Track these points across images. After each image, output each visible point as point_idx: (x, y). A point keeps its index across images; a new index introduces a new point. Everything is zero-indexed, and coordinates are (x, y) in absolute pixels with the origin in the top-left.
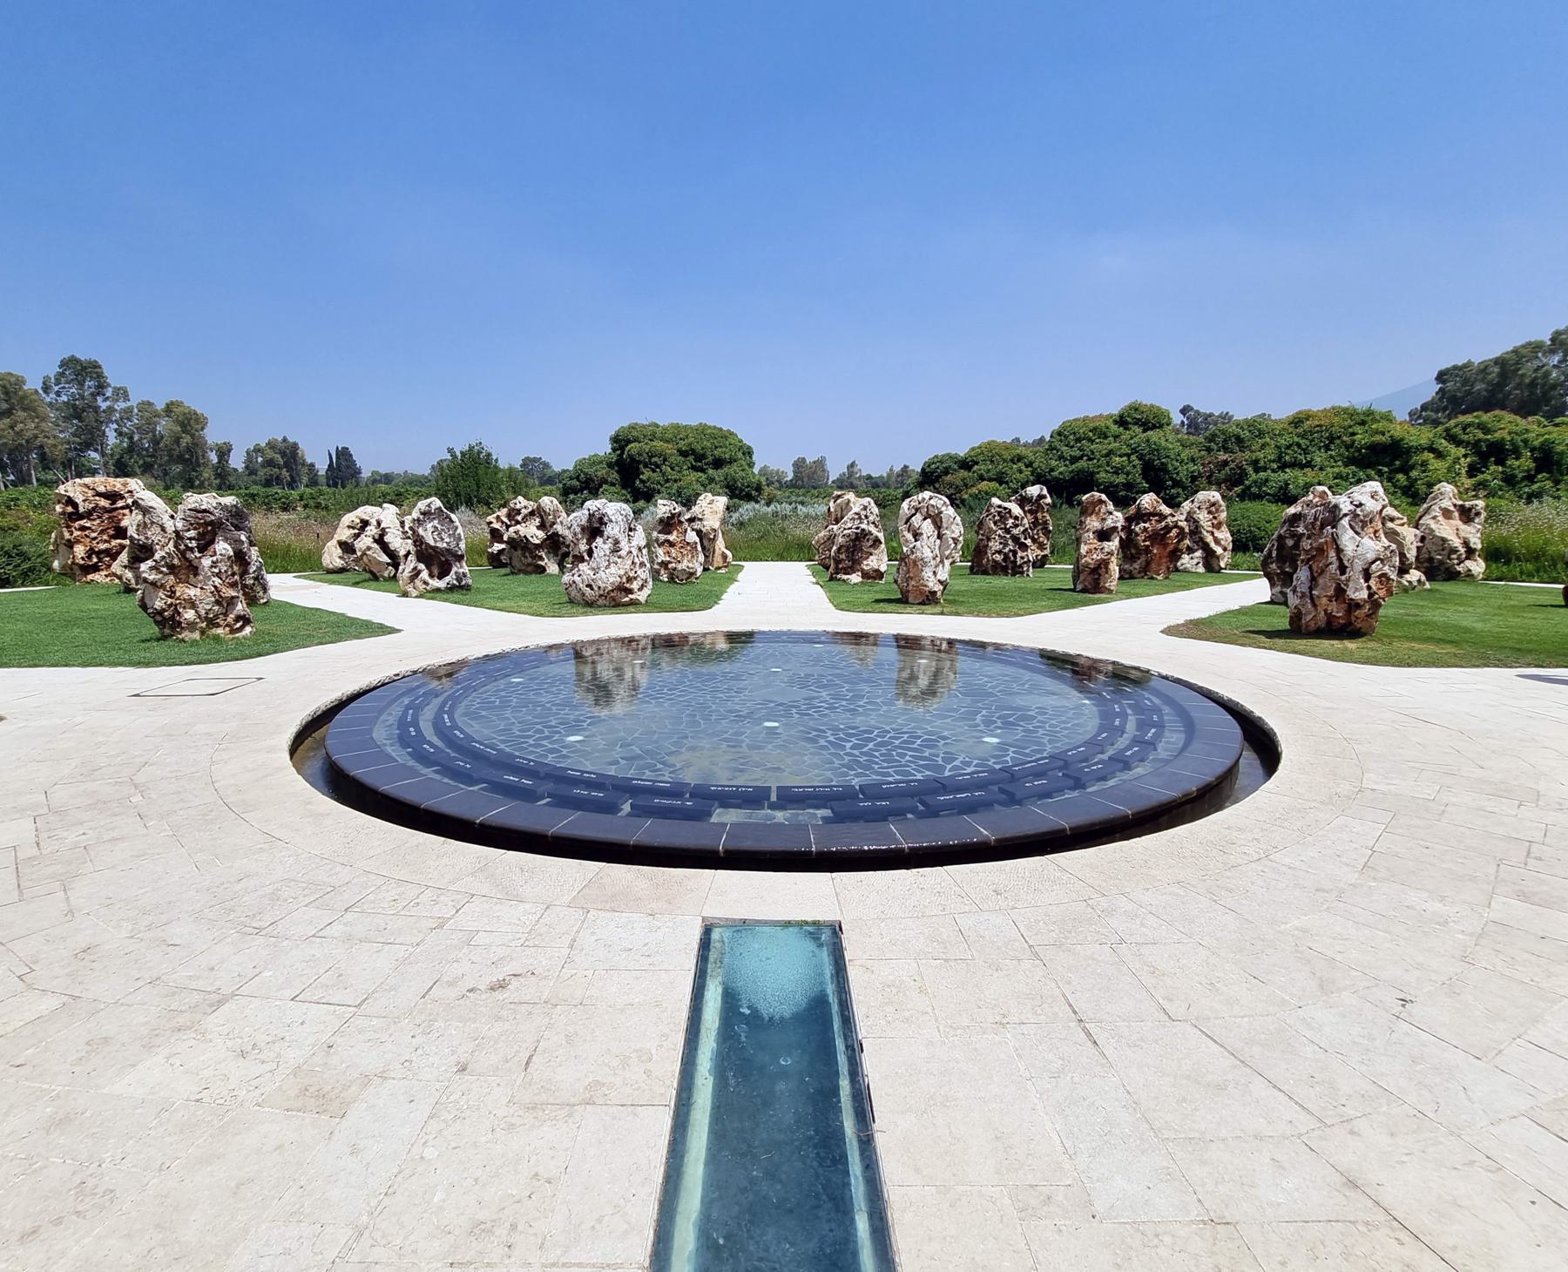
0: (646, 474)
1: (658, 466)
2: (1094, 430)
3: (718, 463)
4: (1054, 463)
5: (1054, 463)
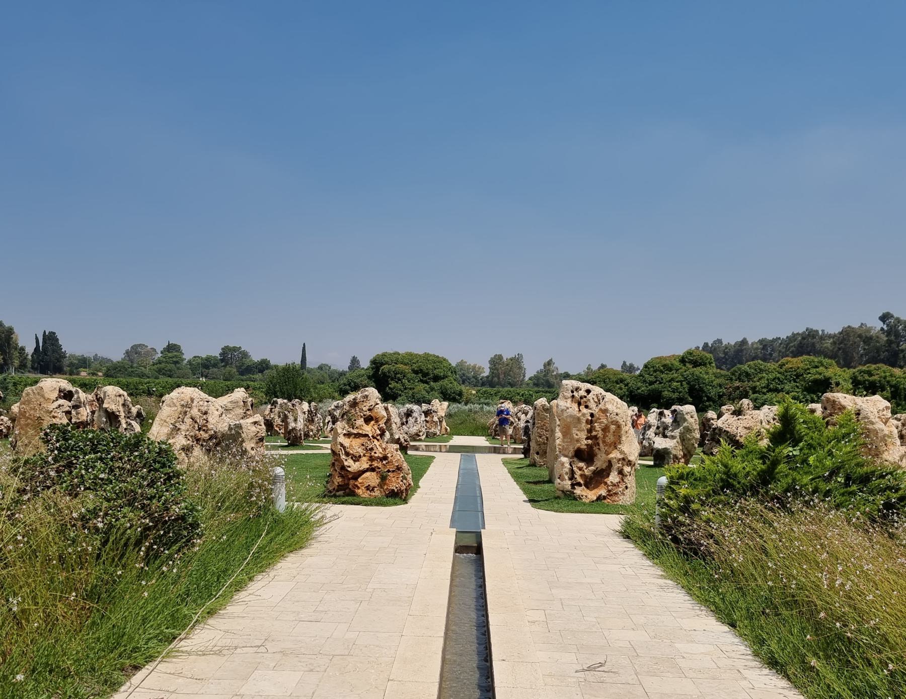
0: (393, 384)
1: (399, 380)
2: (664, 366)
3: (436, 379)
4: (640, 384)
5: (640, 384)
